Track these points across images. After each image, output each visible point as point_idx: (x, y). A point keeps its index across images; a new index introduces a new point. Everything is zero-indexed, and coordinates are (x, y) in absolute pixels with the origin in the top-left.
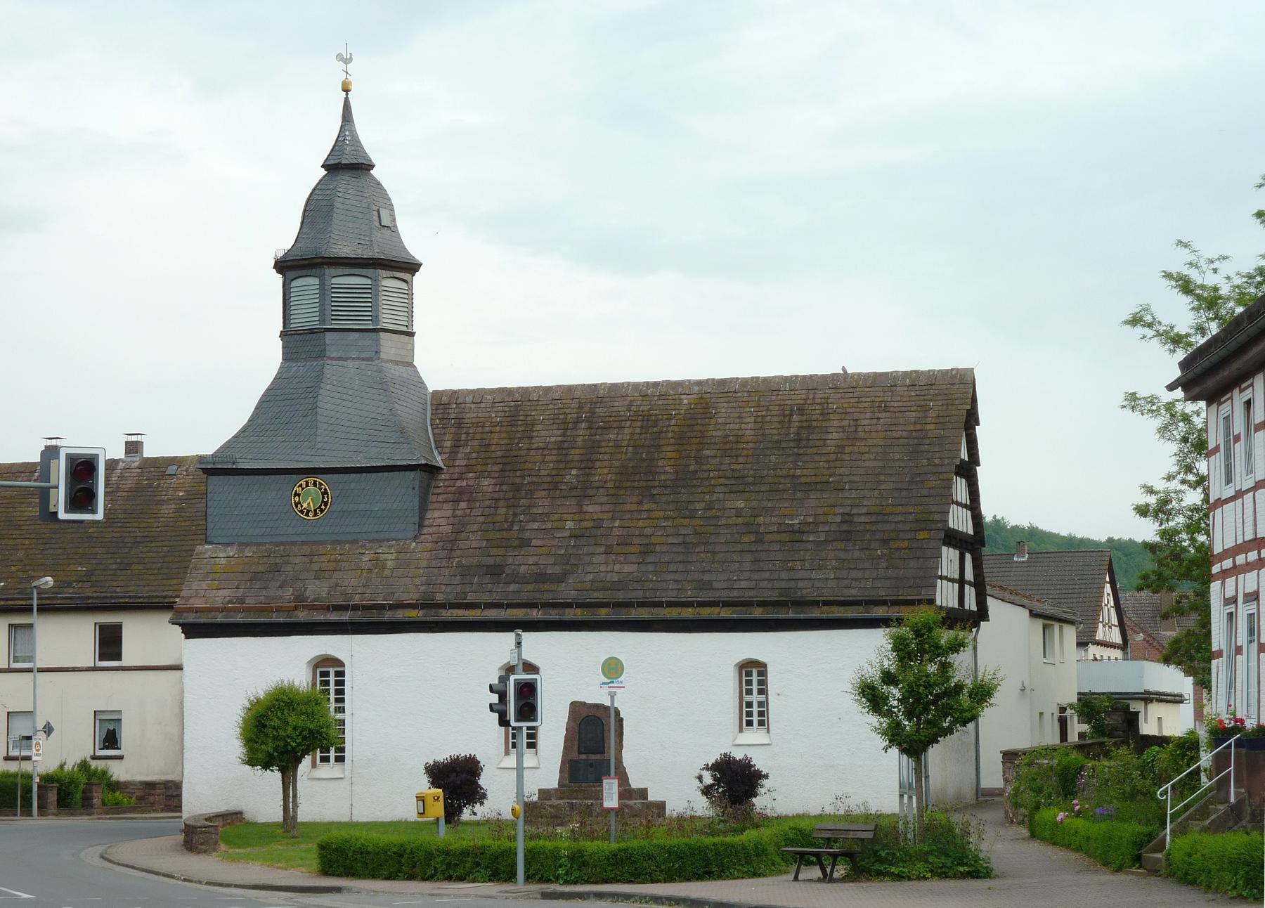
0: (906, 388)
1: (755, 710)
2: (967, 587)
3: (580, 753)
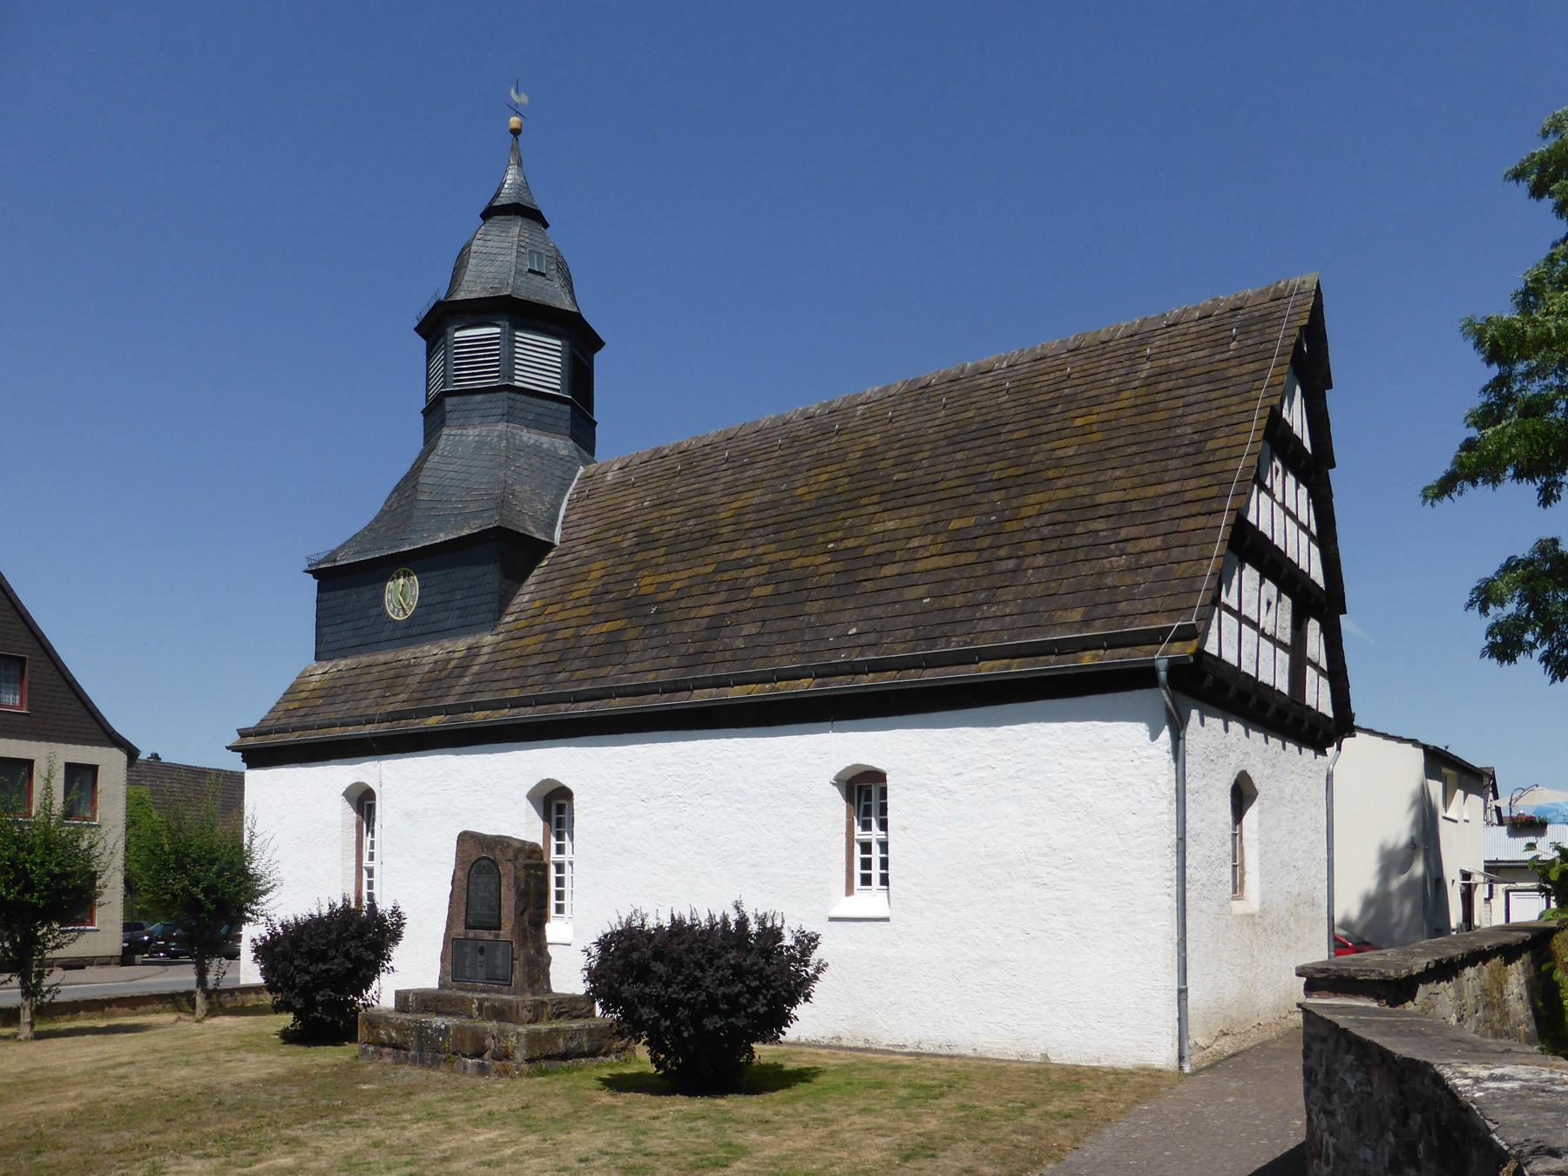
1: (876, 855)
2: (1311, 673)
3: (468, 927)
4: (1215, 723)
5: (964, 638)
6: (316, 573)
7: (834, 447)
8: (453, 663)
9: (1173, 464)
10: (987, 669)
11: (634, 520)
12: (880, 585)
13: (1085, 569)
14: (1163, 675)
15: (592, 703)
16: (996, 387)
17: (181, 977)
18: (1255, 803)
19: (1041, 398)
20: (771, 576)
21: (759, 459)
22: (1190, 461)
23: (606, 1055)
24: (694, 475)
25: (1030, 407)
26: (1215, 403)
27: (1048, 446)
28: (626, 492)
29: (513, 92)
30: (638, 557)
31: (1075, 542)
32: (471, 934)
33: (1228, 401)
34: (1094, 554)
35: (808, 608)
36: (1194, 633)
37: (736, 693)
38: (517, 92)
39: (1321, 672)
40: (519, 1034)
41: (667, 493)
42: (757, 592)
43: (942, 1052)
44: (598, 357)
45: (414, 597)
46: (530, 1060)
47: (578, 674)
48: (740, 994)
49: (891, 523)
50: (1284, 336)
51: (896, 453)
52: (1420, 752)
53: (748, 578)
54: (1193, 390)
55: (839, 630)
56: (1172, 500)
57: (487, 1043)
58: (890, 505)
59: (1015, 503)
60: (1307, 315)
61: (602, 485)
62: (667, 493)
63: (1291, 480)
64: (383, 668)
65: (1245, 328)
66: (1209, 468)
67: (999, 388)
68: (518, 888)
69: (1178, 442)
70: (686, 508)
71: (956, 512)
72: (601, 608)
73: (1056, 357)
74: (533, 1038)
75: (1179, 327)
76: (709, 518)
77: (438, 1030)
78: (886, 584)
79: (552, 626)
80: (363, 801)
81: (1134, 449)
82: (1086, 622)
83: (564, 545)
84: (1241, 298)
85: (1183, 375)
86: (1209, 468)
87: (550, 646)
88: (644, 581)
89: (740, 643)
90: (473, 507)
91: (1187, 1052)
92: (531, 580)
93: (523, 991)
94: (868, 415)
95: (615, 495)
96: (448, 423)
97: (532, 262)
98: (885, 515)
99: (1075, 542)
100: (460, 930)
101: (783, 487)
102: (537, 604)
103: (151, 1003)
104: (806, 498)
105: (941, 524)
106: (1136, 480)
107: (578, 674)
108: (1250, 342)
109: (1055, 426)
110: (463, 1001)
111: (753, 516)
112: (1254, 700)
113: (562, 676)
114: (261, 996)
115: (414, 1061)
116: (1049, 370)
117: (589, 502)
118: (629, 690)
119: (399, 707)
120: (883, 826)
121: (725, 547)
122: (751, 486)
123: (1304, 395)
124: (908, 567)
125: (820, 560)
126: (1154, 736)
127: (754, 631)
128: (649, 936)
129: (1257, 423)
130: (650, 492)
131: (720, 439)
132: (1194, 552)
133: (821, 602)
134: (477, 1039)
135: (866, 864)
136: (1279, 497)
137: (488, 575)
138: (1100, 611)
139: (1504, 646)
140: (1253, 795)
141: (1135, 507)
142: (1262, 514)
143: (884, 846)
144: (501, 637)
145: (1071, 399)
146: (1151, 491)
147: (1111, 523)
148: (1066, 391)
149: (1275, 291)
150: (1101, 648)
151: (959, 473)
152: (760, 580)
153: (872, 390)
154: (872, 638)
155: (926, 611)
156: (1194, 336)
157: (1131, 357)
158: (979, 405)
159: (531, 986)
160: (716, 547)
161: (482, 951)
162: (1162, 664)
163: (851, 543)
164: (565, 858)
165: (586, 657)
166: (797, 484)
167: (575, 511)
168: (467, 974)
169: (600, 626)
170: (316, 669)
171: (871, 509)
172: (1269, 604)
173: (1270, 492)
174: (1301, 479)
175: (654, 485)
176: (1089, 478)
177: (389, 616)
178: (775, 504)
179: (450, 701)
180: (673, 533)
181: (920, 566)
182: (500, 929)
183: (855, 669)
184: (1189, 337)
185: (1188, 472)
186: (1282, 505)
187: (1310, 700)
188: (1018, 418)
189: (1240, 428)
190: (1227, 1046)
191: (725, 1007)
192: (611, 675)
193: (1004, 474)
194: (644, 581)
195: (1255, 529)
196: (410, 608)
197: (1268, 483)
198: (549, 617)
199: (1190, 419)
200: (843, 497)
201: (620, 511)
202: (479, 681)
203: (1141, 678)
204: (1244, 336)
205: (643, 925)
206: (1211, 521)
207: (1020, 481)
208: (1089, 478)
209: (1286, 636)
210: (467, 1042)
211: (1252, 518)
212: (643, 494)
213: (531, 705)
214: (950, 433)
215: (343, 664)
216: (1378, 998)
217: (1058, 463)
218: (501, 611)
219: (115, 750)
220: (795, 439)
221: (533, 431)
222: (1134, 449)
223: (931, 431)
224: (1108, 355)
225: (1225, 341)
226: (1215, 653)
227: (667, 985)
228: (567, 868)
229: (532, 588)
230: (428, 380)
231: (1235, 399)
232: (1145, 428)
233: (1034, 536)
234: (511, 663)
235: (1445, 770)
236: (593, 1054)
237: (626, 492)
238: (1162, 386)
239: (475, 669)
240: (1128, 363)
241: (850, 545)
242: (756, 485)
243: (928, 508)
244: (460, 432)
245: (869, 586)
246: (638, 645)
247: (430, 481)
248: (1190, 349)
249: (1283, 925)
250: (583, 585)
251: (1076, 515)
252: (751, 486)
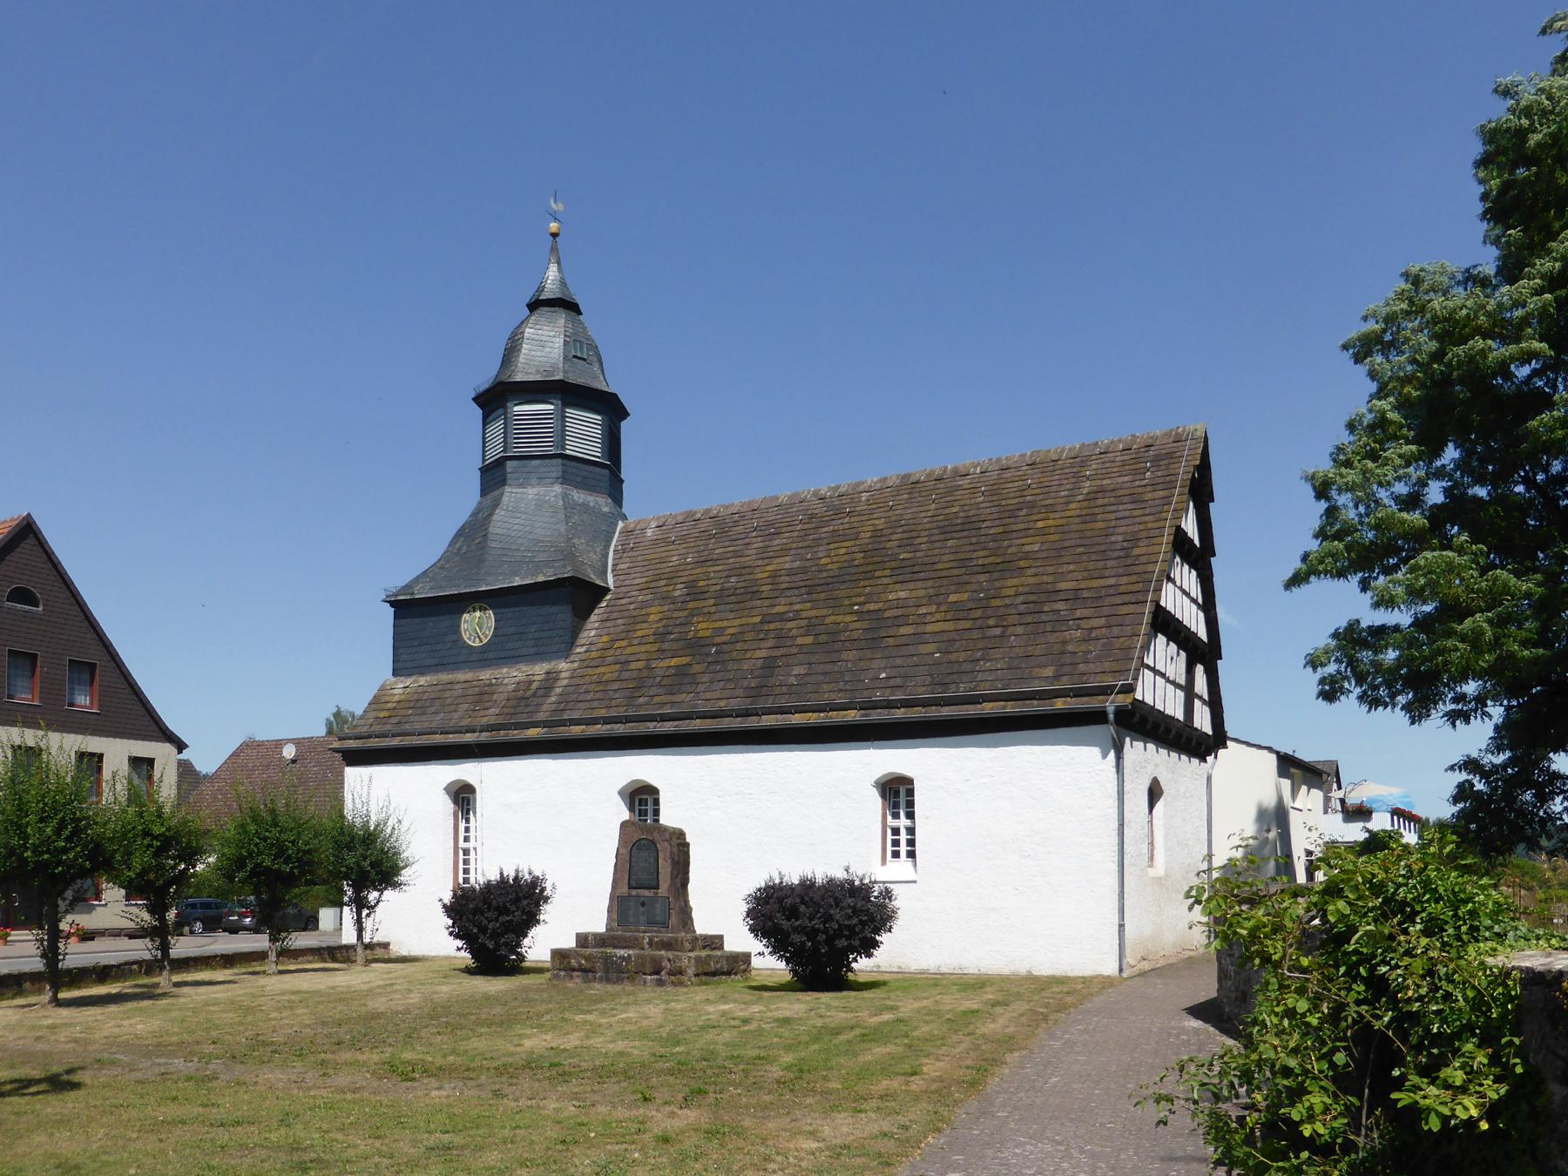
0: (1119, 454)
1: (903, 837)
2: (1197, 703)
3: (630, 887)
4: (1139, 745)
5: (969, 684)
6: (393, 604)
7: (847, 526)
8: (535, 686)
9: (1110, 563)
10: (988, 708)
11: (680, 574)
12: (899, 641)
13: (1052, 638)
14: (1111, 717)
15: (677, 723)
16: (974, 490)
17: (261, 942)
18: (1162, 799)
19: (1009, 502)
20: (809, 629)
21: (784, 530)
22: (1123, 562)
23: (736, 974)
24: (729, 538)
25: (1002, 509)
26: (1138, 520)
27: (1019, 541)
28: (666, 548)
29: (552, 202)
30: (691, 605)
31: (1044, 617)
32: (634, 892)
33: (1144, 519)
34: (1058, 627)
35: (844, 656)
36: (1130, 689)
37: (797, 719)
38: (555, 202)
39: (1204, 702)
40: (690, 957)
41: (706, 553)
42: (800, 641)
44: (623, 424)
45: (489, 629)
46: (697, 975)
47: (656, 699)
48: (856, 925)
49: (902, 593)
50: (1184, 471)
51: (899, 536)
52: (1274, 756)
53: (791, 629)
54: (1121, 507)
55: (872, 674)
56: (1111, 591)
57: (663, 964)
58: (900, 578)
59: (997, 584)
60: (1199, 457)
61: (643, 540)
62: (706, 553)
63: (1186, 567)
64: (465, 685)
65: (1156, 460)
66: (1136, 569)
67: (976, 490)
68: (673, 859)
69: (1113, 547)
70: (726, 567)
71: (953, 588)
72: (665, 646)
73: (1018, 468)
74: (698, 960)
75: (1108, 455)
76: (747, 577)
77: (623, 958)
78: (904, 640)
79: (623, 659)
80: (463, 797)
81: (1081, 549)
82: (1057, 677)
83: (619, 590)
84: (1152, 437)
85: (1112, 494)
86: (1136, 569)
87: (626, 675)
88: (701, 626)
89: (792, 680)
90: (542, 557)
91: (1124, 966)
92: (593, 618)
93: (678, 931)
94: (871, 502)
95: (658, 550)
96: (509, 482)
97: (575, 349)
98: (897, 586)
99: (1044, 617)
100: (624, 890)
101: (809, 556)
102: (605, 639)
103: (306, 955)
104: (829, 567)
105: (942, 597)
106: (1085, 574)
107: (656, 699)
108: (1160, 474)
109: (1022, 526)
110: (636, 939)
111: (787, 579)
112: (1162, 728)
113: (642, 700)
114: (375, 952)
115: (601, 980)
116: (1013, 479)
117: (635, 554)
118: (708, 714)
119: (493, 720)
120: (910, 815)
121: (767, 603)
122: (780, 553)
123: (1195, 506)
124: (921, 629)
125: (848, 618)
126: (1105, 756)
127: (802, 672)
128: (791, 888)
129: (1167, 538)
130: (691, 550)
131: (745, 509)
132: (1128, 630)
133: (855, 652)
135: (896, 843)
136: (1178, 584)
137: (561, 614)
138: (1066, 669)
139: (1330, 692)
140: (1161, 793)
141: (1086, 594)
142: (1171, 599)
143: (911, 831)
144: (576, 665)
145: (1032, 505)
146: (1096, 583)
147: (1069, 605)
148: (1028, 498)
149: (1177, 434)
150: (1069, 696)
151: (952, 557)
152: (801, 631)
153: (872, 479)
154: (898, 681)
155: (937, 663)
156: (1120, 464)
157: (1076, 475)
158: (962, 503)
159: (684, 927)
160: (759, 602)
161: (643, 904)
162: (1111, 709)
163: (872, 607)
164: (470, 845)
165: (660, 685)
166: (820, 555)
167: (622, 561)
168: (631, 920)
169: (668, 661)
170: (395, 683)
171: (885, 581)
172: (1172, 659)
173: (1173, 582)
174: (1192, 566)
175: (692, 544)
176: (1050, 570)
177: (465, 642)
178: (804, 570)
179: (541, 716)
180: (718, 587)
181: (929, 628)
182: (657, 887)
183: (890, 705)
184: (1117, 464)
185: (1121, 571)
186: (1181, 588)
187: (1197, 724)
188: (994, 516)
189: (1155, 540)
190: (1146, 966)
191: (847, 933)
192: (685, 701)
193: (987, 561)
194: (701, 626)
195: (1164, 609)
196: (486, 637)
197: (1172, 576)
198: (619, 650)
199: (1121, 530)
200: (861, 569)
201: (666, 565)
202: (565, 700)
203: (1097, 717)
204: (1155, 469)
205: (782, 883)
206: (1137, 608)
207: (1000, 567)
208: (1050, 570)
209: (1182, 680)
210: (648, 965)
211: (1163, 603)
212: (684, 551)
213: (621, 723)
214: (941, 524)
215: (423, 680)
216: (1206, 1021)
217: (1027, 556)
218: (572, 643)
219: (168, 744)
220: (813, 516)
221: (581, 491)
222: (1081, 549)
223: (925, 520)
224: (1057, 472)
225: (1142, 470)
226: (1141, 699)
227: (811, 919)
228: (472, 852)
229: (596, 625)
230: (484, 443)
231: (1150, 518)
232: (1089, 534)
233: (1014, 611)
234: (592, 687)
235: (1293, 770)
236: (729, 973)
237: (666, 548)
238: (1100, 502)
239: (558, 690)
240: (1074, 480)
241: (872, 608)
242: (784, 553)
243: (930, 583)
244: (520, 490)
245: (890, 641)
246: (706, 678)
247: (499, 531)
248: (1117, 474)
249: (1178, 886)
250: (644, 625)
251: (1043, 597)
252: (780, 553)
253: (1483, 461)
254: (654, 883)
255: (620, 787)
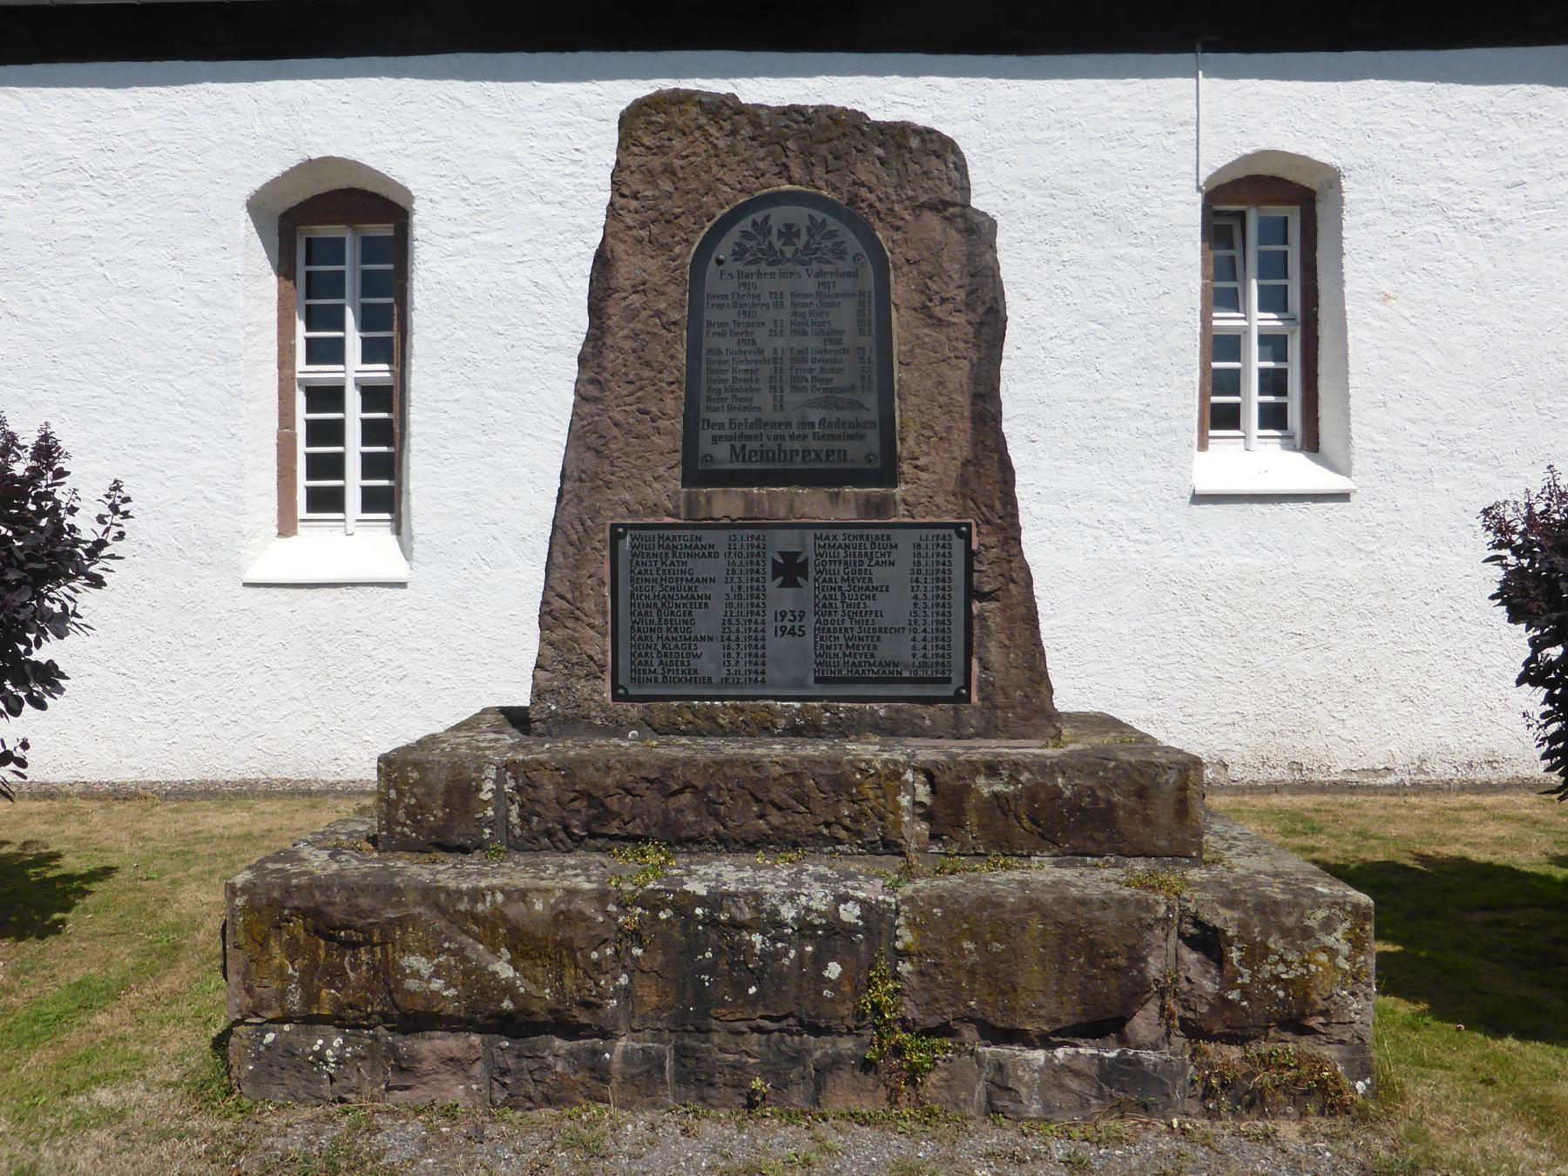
3: (697, 473)
32: (726, 503)
43: (1481, 775)
110: (839, 782)
134: (1094, 952)
161: (791, 570)
182: (888, 473)
210: (1033, 976)
253: (41, 513)
254: (859, 452)
255: (257, 185)
